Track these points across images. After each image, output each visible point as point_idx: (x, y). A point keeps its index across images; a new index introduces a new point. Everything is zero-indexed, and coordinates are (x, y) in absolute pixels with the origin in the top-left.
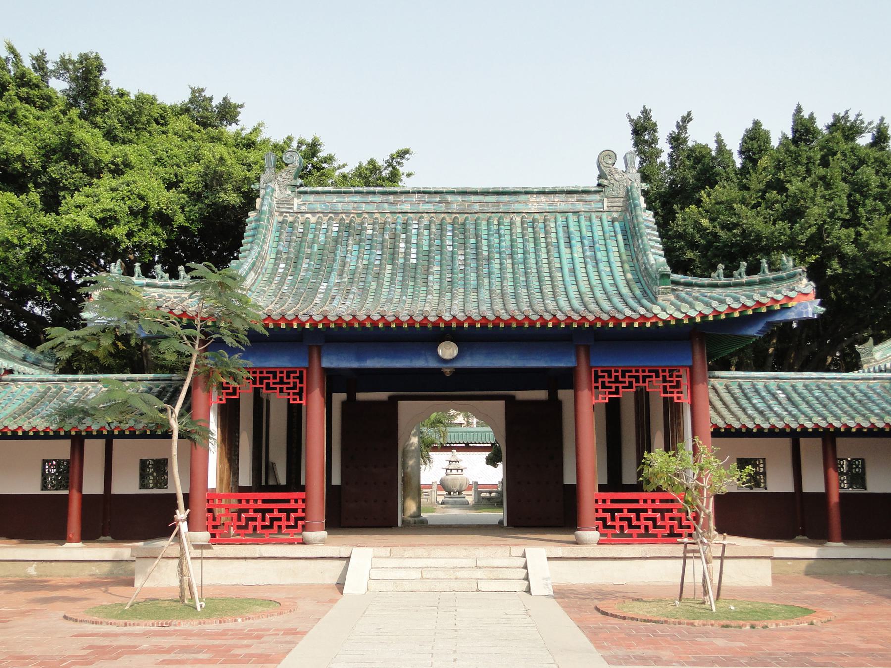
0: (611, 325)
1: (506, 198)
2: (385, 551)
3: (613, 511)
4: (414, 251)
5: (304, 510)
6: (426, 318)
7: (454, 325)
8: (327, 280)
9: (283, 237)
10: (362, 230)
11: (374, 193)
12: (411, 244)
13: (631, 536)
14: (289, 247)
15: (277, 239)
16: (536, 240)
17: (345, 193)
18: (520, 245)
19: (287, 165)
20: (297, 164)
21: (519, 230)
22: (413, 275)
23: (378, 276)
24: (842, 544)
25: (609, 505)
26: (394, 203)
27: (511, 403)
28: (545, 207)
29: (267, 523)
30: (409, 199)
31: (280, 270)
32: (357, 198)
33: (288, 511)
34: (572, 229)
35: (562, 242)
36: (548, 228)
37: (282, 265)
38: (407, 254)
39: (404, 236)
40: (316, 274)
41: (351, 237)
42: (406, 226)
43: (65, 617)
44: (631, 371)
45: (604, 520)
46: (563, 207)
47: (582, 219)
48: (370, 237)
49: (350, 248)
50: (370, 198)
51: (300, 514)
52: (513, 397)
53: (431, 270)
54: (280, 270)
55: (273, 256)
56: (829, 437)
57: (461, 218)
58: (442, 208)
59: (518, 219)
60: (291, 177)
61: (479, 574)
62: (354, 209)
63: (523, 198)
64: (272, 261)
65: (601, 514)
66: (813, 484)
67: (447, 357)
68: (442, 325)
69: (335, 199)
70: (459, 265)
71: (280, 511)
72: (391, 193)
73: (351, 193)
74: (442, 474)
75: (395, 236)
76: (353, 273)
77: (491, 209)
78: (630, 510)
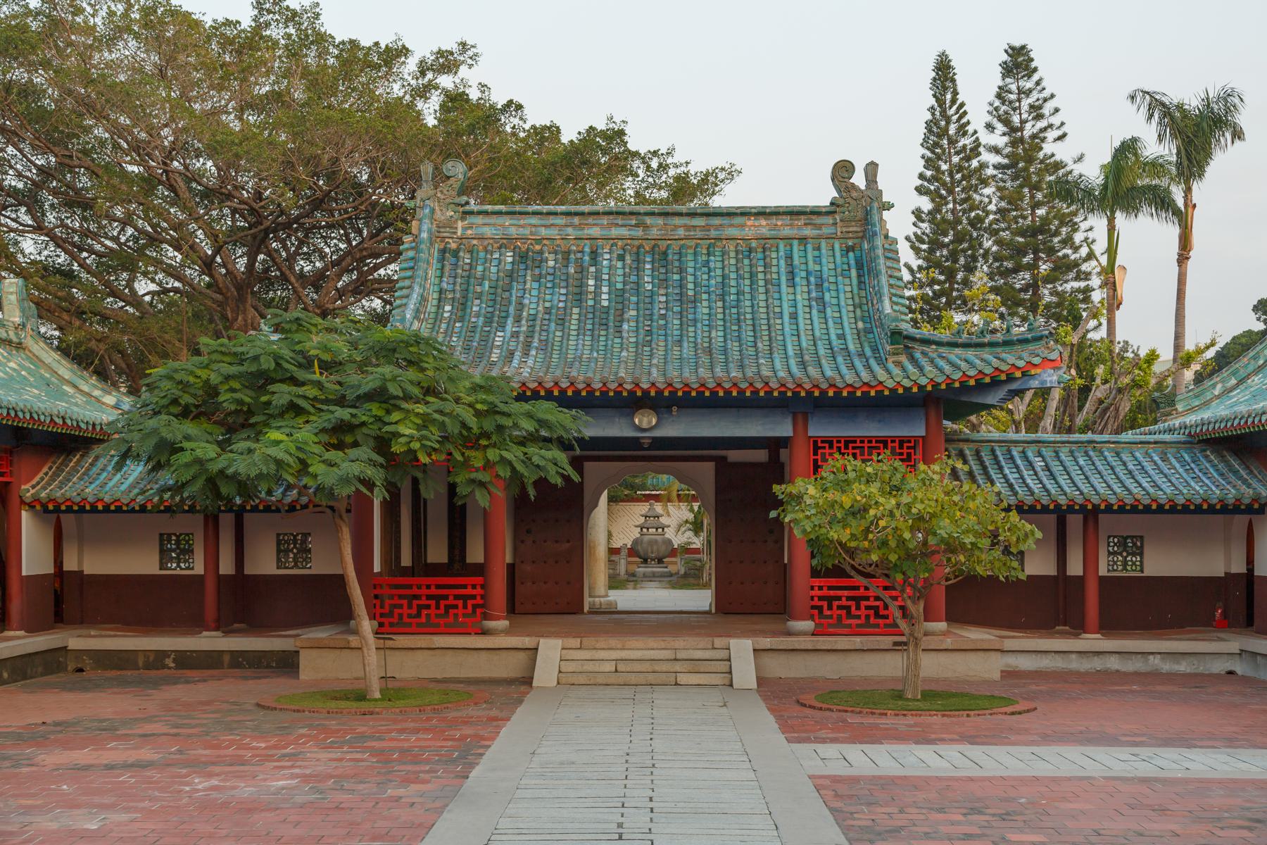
0: (831, 393)
1: (716, 221)
2: (575, 642)
3: (830, 600)
4: (605, 289)
5: (483, 597)
6: (620, 385)
7: (653, 393)
8: (502, 327)
9: (447, 268)
10: (541, 261)
11: (556, 214)
12: (602, 280)
13: (878, 626)
14: (454, 284)
15: (438, 273)
16: (753, 276)
17: (520, 213)
18: (733, 283)
19: (449, 178)
20: (461, 176)
21: (733, 261)
22: (605, 321)
23: (562, 322)
24: (1098, 636)
25: (825, 592)
26: (580, 227)
27: (721, 462)
28: (765, 231)
29: (414, 612)
30: (599, 222)
31: (446, 315)
32: (534, 220)
33: (465, 598)
34: (796, 261)
35: (783, 279)
36: (768, 260)
37: (448, 308)
38: (597, 293)
39: (592, 269)
40: (489, 321)
41: (529, 272)
42: (594, 254)
43: (258, 705)
44: (855, 442)
45: (820, 609)
46: (787, 232)
47: (809, 247)
48: (551, 271)
49: (528, 286)
50: (552, 220)
51: (479, 601)
52: (725, 458)
53: (626, 316)
54: (446, 315)
55: (436, 296)
56: (1091, 514)
57: (663, 244)
58: (639, 233)
59: (731, 246)
60: (454, 193)
61: (678, 667)
62: (531, 233)
63: (738, 220)
64: (435, 302)
65: (816, 602)
66: (1075, 567)
67: (645, 425)
68: (639, 393)
69: (507, 221)
70: (659, 309)
71: (457, 597)
72: (576, 214)
73: (528, 213)
74: (636, 533)
75: (581, 270)
76: (533, 318)
77: (699, 234)
78: (849, 598)
